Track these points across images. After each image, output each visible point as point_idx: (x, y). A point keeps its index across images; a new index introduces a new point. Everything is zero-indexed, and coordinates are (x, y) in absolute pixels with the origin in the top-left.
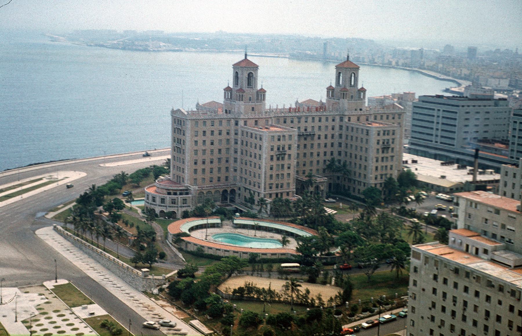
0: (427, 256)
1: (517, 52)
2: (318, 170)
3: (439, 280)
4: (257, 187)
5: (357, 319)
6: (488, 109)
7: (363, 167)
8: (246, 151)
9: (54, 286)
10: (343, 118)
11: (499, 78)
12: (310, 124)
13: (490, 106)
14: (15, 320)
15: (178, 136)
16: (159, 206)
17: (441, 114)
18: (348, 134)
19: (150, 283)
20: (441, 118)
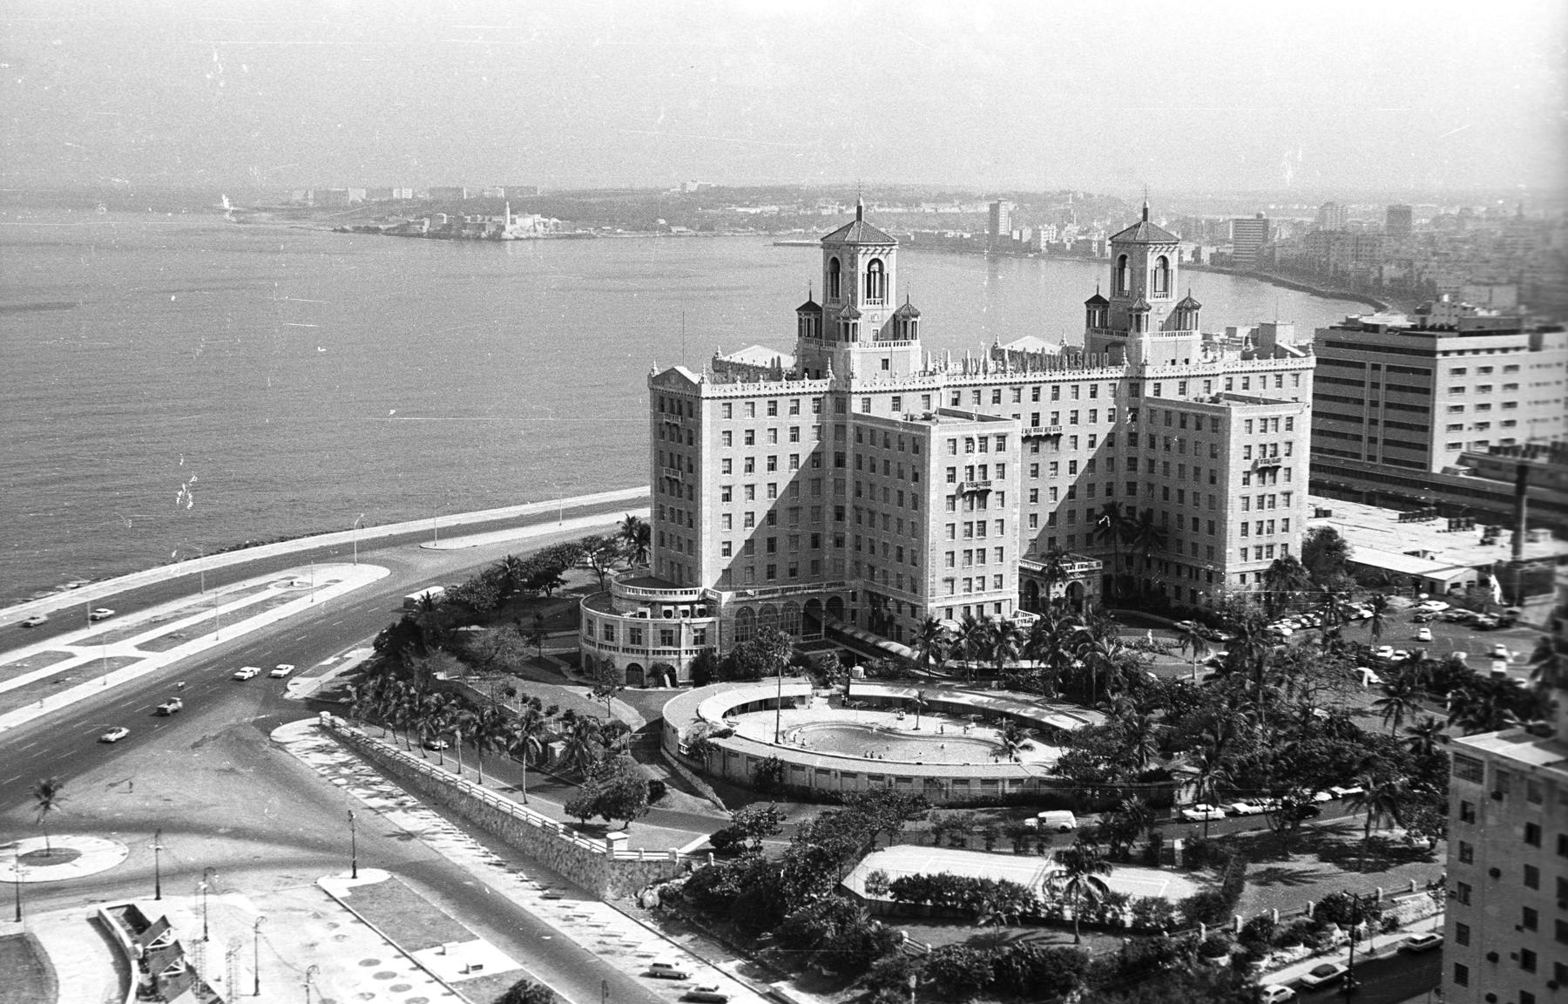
0: (1505, 770)
1: (1520, 216)
2: (1071, 538)
3: (1544, 841)
4: (907, 591)
5: (1273, 965)
6: (1511, 358)
7: (1204, 525)
8: (872, 486)
9: (350, 889)
10: (1138, 385)
11: (1487, 284)
12: (1045, 407)
13: (1517, 349)
14: (253, 991)
15: (683, 448)
16: (626, 650)
17: (1383, 377)
18: (860, 505)
19: (632, 873)
20: (1383, 388)
